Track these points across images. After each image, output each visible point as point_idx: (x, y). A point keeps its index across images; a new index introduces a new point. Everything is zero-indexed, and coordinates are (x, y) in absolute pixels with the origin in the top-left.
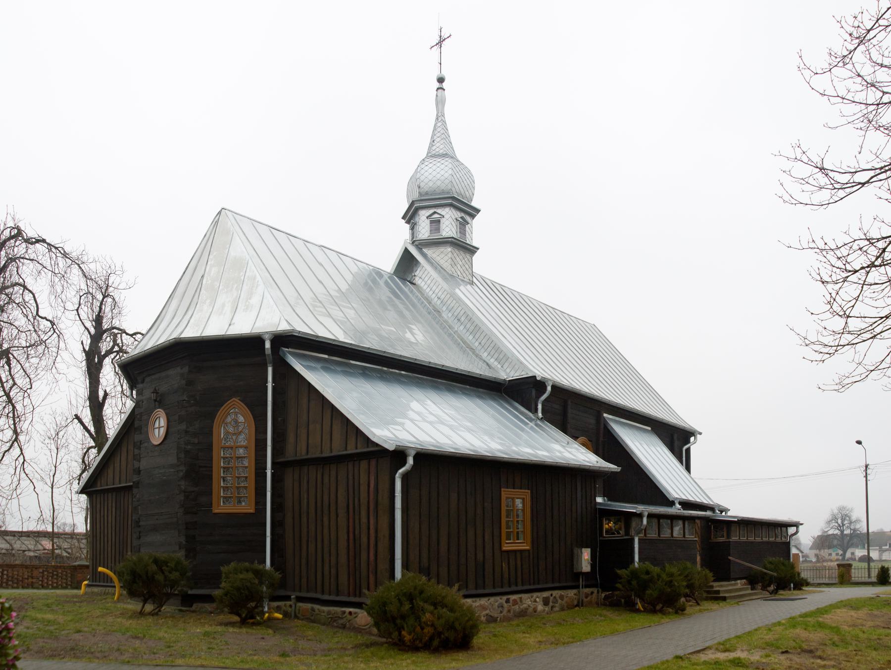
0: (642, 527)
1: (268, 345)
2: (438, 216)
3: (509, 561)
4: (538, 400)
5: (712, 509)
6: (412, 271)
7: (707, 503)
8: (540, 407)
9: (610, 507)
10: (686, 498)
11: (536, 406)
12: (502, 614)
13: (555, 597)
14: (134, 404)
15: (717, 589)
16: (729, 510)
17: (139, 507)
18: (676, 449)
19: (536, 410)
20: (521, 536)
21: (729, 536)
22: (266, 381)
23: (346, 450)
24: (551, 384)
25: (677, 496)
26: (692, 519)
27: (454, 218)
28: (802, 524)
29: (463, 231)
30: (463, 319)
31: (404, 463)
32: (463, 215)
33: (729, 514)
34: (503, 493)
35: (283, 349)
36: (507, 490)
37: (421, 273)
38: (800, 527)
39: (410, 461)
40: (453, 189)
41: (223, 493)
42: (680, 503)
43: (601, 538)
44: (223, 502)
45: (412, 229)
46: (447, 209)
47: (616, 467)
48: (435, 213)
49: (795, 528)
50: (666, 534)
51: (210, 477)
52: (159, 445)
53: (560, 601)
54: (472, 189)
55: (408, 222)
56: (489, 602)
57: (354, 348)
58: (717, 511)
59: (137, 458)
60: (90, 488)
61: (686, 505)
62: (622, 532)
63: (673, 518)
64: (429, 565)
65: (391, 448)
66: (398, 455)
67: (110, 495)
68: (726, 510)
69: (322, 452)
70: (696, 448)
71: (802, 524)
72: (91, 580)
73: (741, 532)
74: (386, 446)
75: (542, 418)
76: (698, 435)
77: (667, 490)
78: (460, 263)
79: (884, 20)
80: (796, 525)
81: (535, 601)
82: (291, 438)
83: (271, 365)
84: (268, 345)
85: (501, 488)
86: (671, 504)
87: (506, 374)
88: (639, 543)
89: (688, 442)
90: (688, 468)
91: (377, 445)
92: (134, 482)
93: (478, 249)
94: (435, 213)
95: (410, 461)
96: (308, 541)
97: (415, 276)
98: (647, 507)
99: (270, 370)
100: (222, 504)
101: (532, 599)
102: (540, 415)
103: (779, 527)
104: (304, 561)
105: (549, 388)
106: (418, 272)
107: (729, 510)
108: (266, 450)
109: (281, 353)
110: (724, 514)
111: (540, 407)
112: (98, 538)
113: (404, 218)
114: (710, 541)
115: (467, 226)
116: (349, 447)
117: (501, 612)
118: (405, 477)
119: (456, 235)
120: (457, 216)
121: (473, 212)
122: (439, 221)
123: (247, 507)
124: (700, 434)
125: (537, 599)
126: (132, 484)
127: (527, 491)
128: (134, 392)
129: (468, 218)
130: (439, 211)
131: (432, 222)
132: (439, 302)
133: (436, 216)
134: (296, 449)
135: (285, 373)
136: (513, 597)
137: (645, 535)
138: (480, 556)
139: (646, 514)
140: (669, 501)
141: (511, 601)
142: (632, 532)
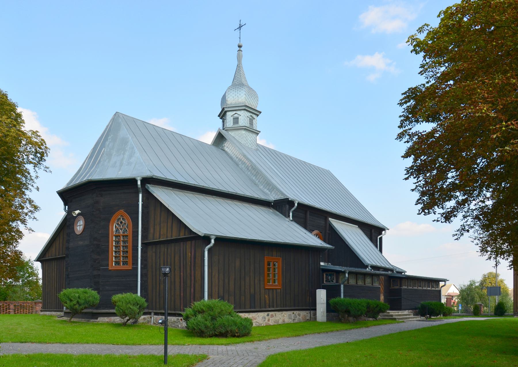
0: (346, 279)
1: (139, 183)
2: (238, 115)
3: (269, 294)
4: (290, 211)
5: (392, 270)
6: (223, 144)
7: (388, 267)
8: (291, 214)
9: (327, 267)
10: (376, 264)
11: (289, 213)
12: (265, 322)
13: (295, 315)
14: (67, 214)
15: (392, 314)
16: (406, 272)
17: (69, 268)
18: (374, 238)
19: (289, 216)
20: (277, 282)
21: (401, 286)
22: (138, 201)
23: (179, 236)
24: (297, 202)
25: (369, 263)
26: (378, 275)
27: (246, 116)
28: (448, 280)
29: (251, 123)
30: (250, 168)
31: (209, 242)
32: (251, 114)
33: (406, 274)
34: (265, 259)
35: (147, 185)
36: (268, 257)
37: (228, 144)
38: (447, 282)
39: (213, 241)
40: (246, 101)
41: (115, 259)
42: (371, 267)
43: (323, 284)
44: (115, 264)
45: (223, 122)
46: (243, 111)
47: (332, 246)
48: (236, 113)
49: (444, 282)
50: (360, 283)
51: (108, 251)
52: (80, 234)
53: (298, 317)
54: (257, 101)
55: (221, 118)
56: (257, 315)
57: (186, 184)
58: (395, 272)
59: (68, 241)
60: (42, 258)
61: (374, 267)
62: (335, 281)
63: (365, 275)
64: (224, 295)
65: (203, 235)
66: (206, 239)
67: (53, 262)
68: (405, 272)
69: (167, 237)
70: (386, 237)
71: (448, 280)
72: (43, 308)
73: (409, 284)
74: (200, 234)
75: (292, 220)
76: (387, 230)
77: (363, 259)
78: (250, 139)
79: (251, 80)
80: (444, 281)
81: (284, 316)
82: (151, 231)
83: (141, 193)
84: (139, 183)
85: (264, 256)
86: (367, 267)
87: (272, 197)
88: (344, 287)
89: (381, 234)
90: (381, 250)
91: (195, 233)
92: (66, 255)
93: (260, 132)
94: (236, 113)
95: (213, 241)
96: (160, 284)
97: (224, 146)
98: (348, 268)
99: (140, 196)
100: (114, 265)
101: (282, 315)
102: (291, 218)
103: (436, 282)
104: (158, 294)
105: (296, 205)
106: (226, 144)
107: (406, 272)
108: (138, 237)
109: (146, 187)
110: (403, 274)
111: (291, 214)
112: (47, 285)
113: (219, 116)
114: (390, 288)
115: (253, 120)
116: (181, 235)
117: (264, 321)
118: (210, 250)
119: (247, 124)
120: (248, 115)
121: (257, 113)
122: (238, 118)
123: (129, 267)
124: (388, 229)
125: (285, 315)
126: (65, 256)
127: (279, 258)
128: (67, 207)
129: (254, 116)
130: (238, 112)
131: (234, 119)
132: (237, 160)
133: (236, 115)
134: (155, 236)
135: (149, 197)
136: (270, 313)
137: (348, 283)
138: (252, 291)
139: (348, 271)
140: (365, 265)
141: (270, 315)
142: (340, 281)
